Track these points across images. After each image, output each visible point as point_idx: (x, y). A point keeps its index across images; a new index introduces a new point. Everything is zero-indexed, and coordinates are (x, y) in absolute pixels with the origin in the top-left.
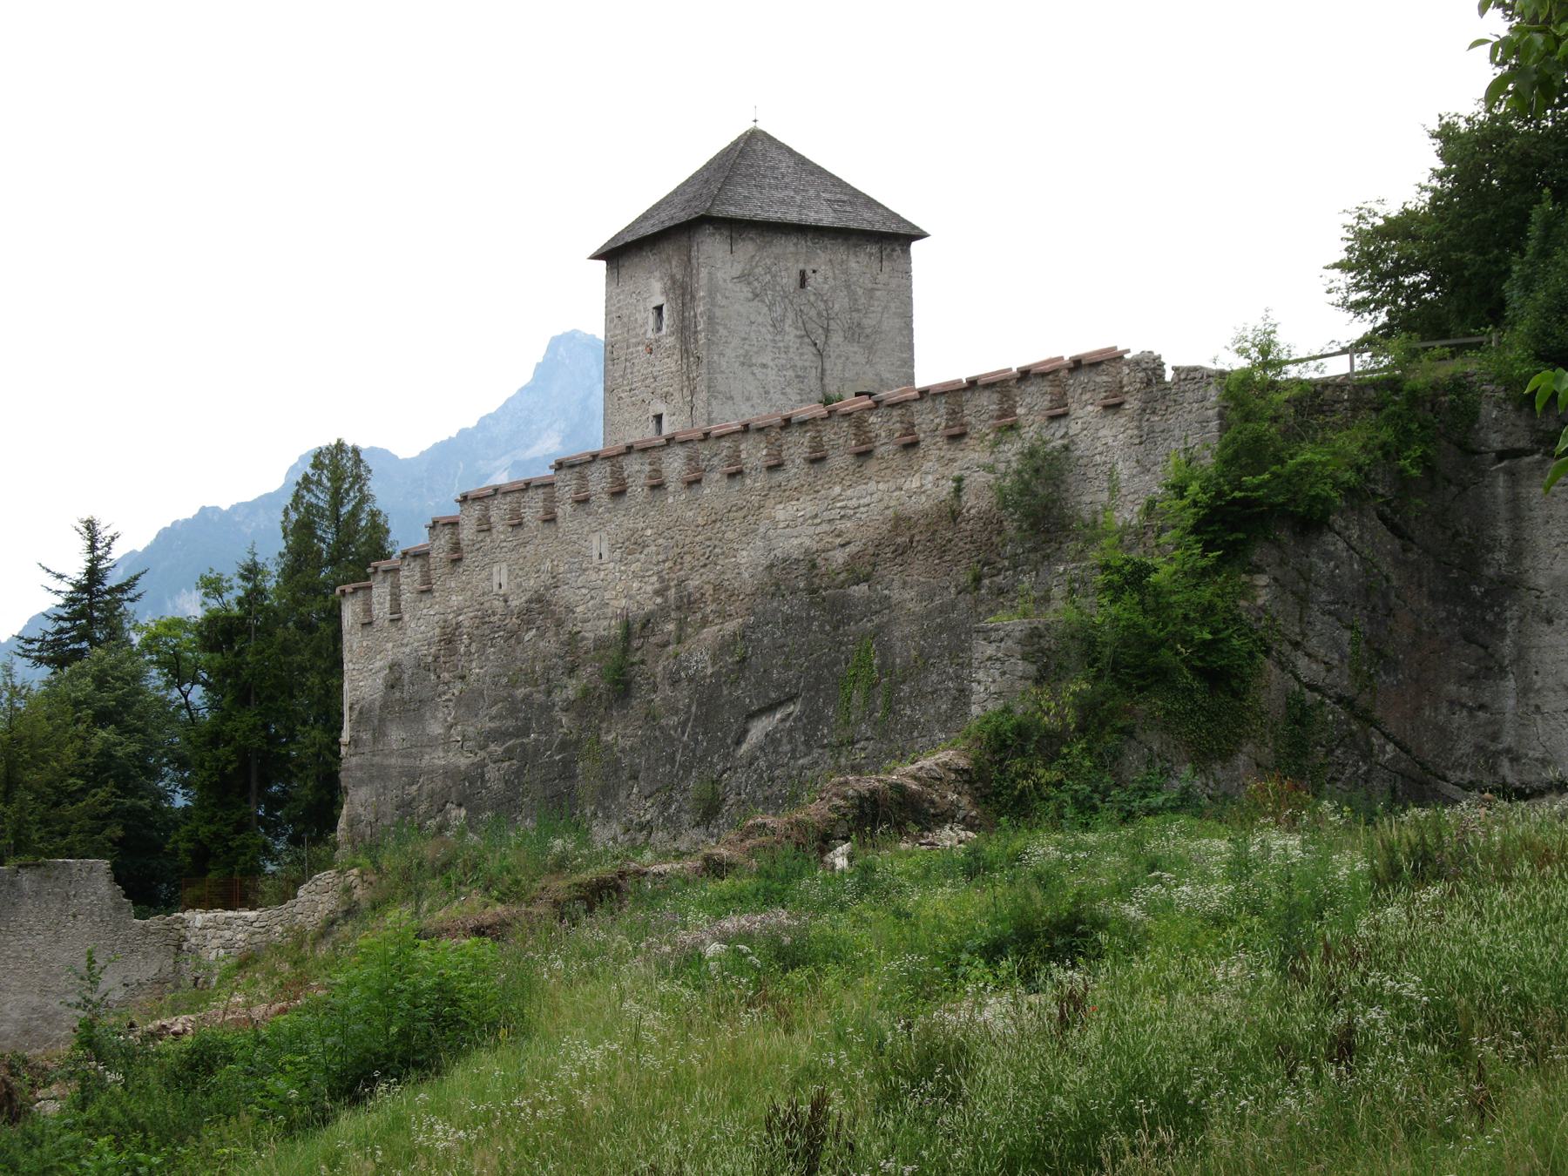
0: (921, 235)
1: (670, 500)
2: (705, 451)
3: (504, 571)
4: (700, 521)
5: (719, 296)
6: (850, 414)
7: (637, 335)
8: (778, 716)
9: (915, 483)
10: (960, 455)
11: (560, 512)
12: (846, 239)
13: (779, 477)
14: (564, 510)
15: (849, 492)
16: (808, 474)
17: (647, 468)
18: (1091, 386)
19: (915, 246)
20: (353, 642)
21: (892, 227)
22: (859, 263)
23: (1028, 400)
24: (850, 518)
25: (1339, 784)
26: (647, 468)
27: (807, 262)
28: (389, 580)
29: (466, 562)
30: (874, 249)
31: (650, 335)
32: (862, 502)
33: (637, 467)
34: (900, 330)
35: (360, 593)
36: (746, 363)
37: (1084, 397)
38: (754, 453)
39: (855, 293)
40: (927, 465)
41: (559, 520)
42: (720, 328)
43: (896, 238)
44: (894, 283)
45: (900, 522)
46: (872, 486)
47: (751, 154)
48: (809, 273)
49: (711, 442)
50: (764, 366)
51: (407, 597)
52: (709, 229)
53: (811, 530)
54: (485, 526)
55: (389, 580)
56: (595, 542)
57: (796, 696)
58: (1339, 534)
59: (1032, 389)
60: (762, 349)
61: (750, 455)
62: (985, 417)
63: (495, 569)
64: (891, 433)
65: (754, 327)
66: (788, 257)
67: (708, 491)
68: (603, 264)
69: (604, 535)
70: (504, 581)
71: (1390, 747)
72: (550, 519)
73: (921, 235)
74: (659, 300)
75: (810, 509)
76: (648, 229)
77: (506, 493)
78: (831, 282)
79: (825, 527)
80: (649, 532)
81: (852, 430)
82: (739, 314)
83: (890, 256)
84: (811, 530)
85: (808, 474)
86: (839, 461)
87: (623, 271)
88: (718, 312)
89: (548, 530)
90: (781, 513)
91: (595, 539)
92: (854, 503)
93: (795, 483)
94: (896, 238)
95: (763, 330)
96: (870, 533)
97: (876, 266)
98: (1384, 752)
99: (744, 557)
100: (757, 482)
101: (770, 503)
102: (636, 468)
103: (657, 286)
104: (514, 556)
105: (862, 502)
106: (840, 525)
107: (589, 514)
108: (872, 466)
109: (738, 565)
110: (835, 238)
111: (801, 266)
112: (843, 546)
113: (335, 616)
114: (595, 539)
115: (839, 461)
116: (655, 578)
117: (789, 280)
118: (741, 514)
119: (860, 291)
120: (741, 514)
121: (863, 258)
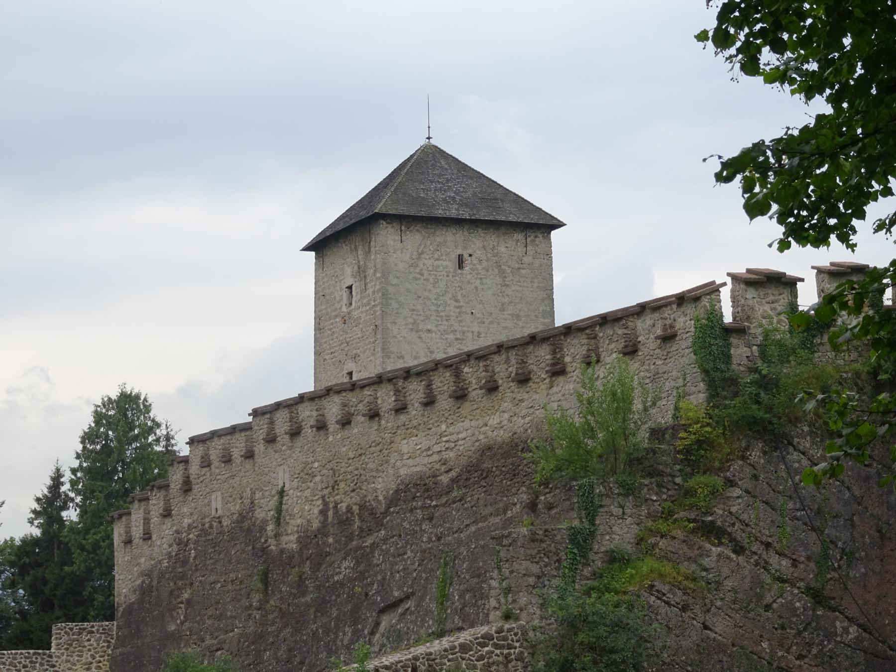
0: (559, 225)
1: (331, 439)
2: (352, 398)
3: (219, 499)
4: (351, 455)
5: (391, 277)
6: (451, 366)
7: (336, 309)
8: (400, 611)
9: (494, 421)
10: (526, 396)
11: (256, 450)
12: (497, 229)
13: (403, 418)
14: (260, 448)
15: (451, 429)
16: (423, 415)
17: (315, 413)
18: (615, 338)
19: (555, 235)
20: (120, 556)
21: (534, 219)
22: (508, 247)
23: (572, 351)
24: (452, 449)
25: (806, 660)
26: (315, 413)
27: (465, 248)
28: (143, 508)
29: (195, 491)
30: (519, 236)
31: (344, 309)
32: (461, 436)
33: (307, 413)
34: (543, 300)
35: (124, 519)
36: (415, 329)
37: (611, 347)
38: (386, 398)
39: (504, 272)
40: (505, 405)
41: (256, 457)
42: (393, 302)
43: (543, 226)
44: (537, 263)
45: (487, 450)
46: (467, 424)
47: (429, 162)
48: (466, 256)
49: (357, 391)
50: (429, 331)
51: (155, 520)
52: (383, 223)
53: (426, 460)
54: (206, 463)
55: (143, 508)
56: (281, 474)
57: (413, 594)
58: (803, 454)
59: (576, 341)
60: (427, 318)
61: (383, 401)
62: (543, 365)
63: (213, 497)
64: (479, 379)
65: (420, 301)
66: (452, 241)
67: (356, 431)
68: (313, 253)
69: (286, 468)
70: (219, 506)
71: (853, 630)
72: (249, 455)
73: (559, 225)
74: (349, 281)
75: (425, 443)
76: (341, 226)
77: (220, 436)
78: (485, 264)
79: (436, 457)
80: (316, 465)
81: (452, 379)
82: (408, 291)
83: (533, 241)
84: (426, 460)
85: (423, 415)
86: (444, 403)
87: (326, 259)
88: (391, 289)
89: (248, 465)
90: (405, 447)
91: (280, 471)
92: (454, 437)
93: (415, 422)
94: (543, 226)
95: (428, 303)
96: (464, 461)
97: (521, 250)
98: (848, 633)
99: (379, 485)
100: (388, 421)
101: (398, 439)
102: (307, 413)
103: (348, 270)
104: (226, 486)
105: (461, 436)
106: (445, 455)
107: (276, 452)
108: (467, 407)
109: (376, 490)
110: (487, 229)
111: (459, 252)
112: (447, 472)
113: (109, 537)
114: (280, 471)
115: (444, 403)
116: (320, 502)
117: (450, 264)
118: (379, 448)
119: (508, 270)
120: (379, 448)
121: (511, 243)
